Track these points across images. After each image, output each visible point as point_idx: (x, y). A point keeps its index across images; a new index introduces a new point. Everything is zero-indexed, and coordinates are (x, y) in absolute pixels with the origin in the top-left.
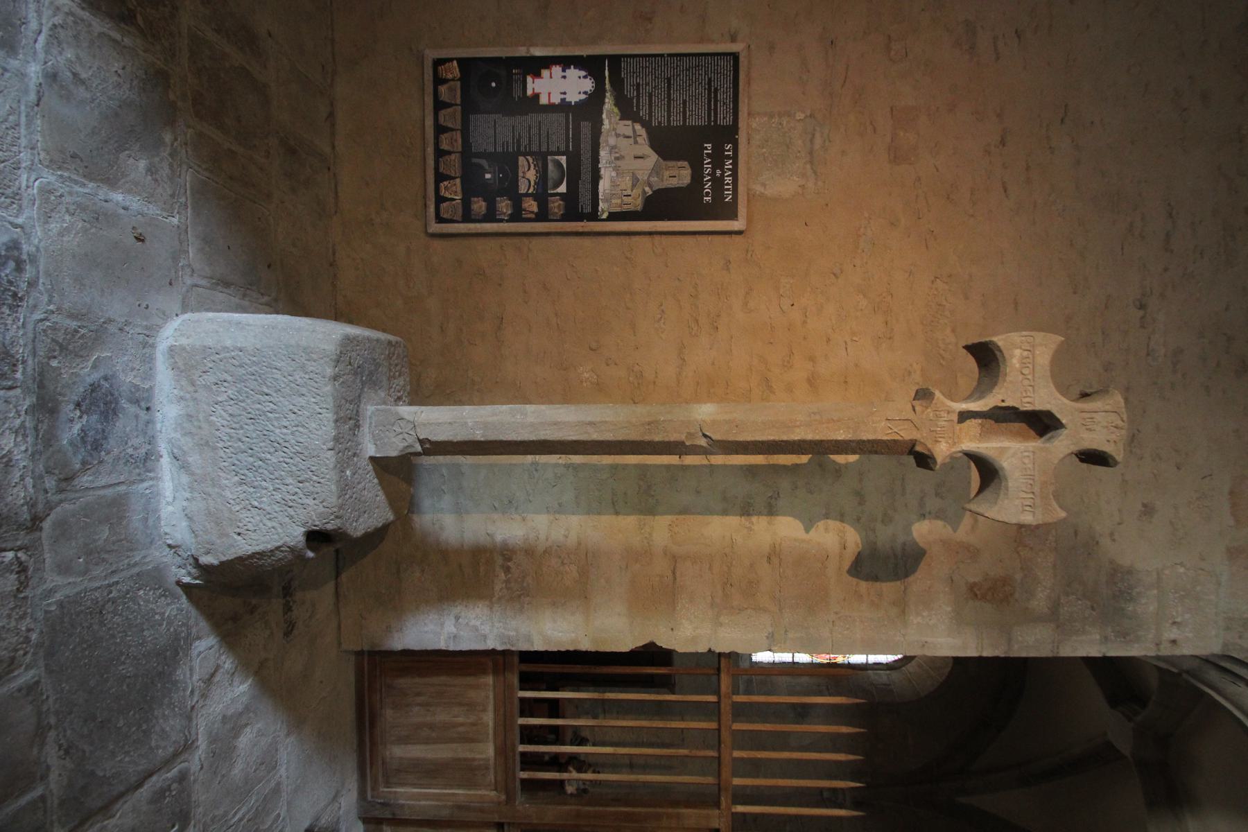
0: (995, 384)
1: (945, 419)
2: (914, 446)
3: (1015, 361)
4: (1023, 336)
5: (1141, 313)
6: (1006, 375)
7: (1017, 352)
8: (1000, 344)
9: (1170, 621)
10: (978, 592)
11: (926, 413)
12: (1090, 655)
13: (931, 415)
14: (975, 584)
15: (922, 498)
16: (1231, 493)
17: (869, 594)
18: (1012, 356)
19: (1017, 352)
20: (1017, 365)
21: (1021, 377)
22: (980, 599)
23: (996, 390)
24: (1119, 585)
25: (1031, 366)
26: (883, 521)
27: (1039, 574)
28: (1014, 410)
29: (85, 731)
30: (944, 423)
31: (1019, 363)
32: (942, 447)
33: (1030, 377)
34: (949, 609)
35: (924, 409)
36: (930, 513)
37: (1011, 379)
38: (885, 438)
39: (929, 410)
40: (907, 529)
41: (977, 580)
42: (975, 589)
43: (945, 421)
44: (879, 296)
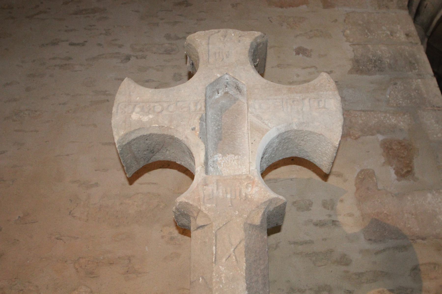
0: (172, 138)
1: (215, 188)
2: (252, 226)
3: (145, 119)
4: (117, 112)
5: (133, 59)
6: (161, 127)
7: (135, 116)
8: (122, 133)
9: (392, 37)
10: (405, 170)
11: (206, 212)
12: (437, 85)
13: (209, 205)
14: (397, 173)
15: (316, 225)
16: (281, 7)
17: (436, 278)
18: (139, 121)
19: (135, 116)
20: (151, 116)
21: (164, 112)
22: (411, 167)
23: (180, 136)
24: (370, 68)
25: (152, 105)
26: (347, 264)
27: (374, 122)
28: (205, 117)
29: (248, 203)
30: (220, 191)
31: (148, 115)
32: (254, 192)
33: (165, 105)
34: (429, 195)
35: (200, 214)
36: (330, 216)
37: (166, 122)
38: (244, 265)
39: (203, 208)
40: (350, 238)
41: (393, 172)
42: (403, 173)
43: (217, 189)
44: (78, 272)
